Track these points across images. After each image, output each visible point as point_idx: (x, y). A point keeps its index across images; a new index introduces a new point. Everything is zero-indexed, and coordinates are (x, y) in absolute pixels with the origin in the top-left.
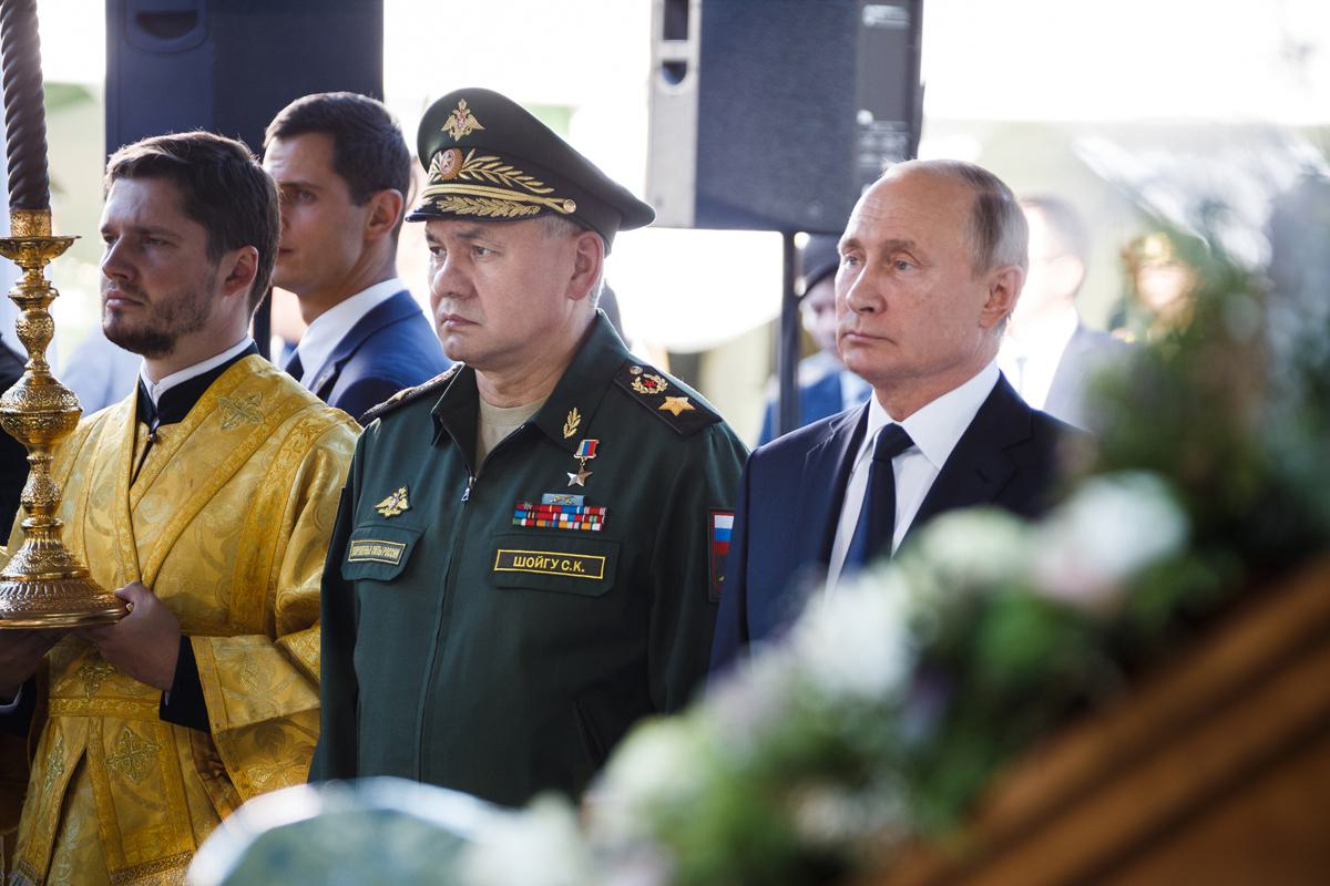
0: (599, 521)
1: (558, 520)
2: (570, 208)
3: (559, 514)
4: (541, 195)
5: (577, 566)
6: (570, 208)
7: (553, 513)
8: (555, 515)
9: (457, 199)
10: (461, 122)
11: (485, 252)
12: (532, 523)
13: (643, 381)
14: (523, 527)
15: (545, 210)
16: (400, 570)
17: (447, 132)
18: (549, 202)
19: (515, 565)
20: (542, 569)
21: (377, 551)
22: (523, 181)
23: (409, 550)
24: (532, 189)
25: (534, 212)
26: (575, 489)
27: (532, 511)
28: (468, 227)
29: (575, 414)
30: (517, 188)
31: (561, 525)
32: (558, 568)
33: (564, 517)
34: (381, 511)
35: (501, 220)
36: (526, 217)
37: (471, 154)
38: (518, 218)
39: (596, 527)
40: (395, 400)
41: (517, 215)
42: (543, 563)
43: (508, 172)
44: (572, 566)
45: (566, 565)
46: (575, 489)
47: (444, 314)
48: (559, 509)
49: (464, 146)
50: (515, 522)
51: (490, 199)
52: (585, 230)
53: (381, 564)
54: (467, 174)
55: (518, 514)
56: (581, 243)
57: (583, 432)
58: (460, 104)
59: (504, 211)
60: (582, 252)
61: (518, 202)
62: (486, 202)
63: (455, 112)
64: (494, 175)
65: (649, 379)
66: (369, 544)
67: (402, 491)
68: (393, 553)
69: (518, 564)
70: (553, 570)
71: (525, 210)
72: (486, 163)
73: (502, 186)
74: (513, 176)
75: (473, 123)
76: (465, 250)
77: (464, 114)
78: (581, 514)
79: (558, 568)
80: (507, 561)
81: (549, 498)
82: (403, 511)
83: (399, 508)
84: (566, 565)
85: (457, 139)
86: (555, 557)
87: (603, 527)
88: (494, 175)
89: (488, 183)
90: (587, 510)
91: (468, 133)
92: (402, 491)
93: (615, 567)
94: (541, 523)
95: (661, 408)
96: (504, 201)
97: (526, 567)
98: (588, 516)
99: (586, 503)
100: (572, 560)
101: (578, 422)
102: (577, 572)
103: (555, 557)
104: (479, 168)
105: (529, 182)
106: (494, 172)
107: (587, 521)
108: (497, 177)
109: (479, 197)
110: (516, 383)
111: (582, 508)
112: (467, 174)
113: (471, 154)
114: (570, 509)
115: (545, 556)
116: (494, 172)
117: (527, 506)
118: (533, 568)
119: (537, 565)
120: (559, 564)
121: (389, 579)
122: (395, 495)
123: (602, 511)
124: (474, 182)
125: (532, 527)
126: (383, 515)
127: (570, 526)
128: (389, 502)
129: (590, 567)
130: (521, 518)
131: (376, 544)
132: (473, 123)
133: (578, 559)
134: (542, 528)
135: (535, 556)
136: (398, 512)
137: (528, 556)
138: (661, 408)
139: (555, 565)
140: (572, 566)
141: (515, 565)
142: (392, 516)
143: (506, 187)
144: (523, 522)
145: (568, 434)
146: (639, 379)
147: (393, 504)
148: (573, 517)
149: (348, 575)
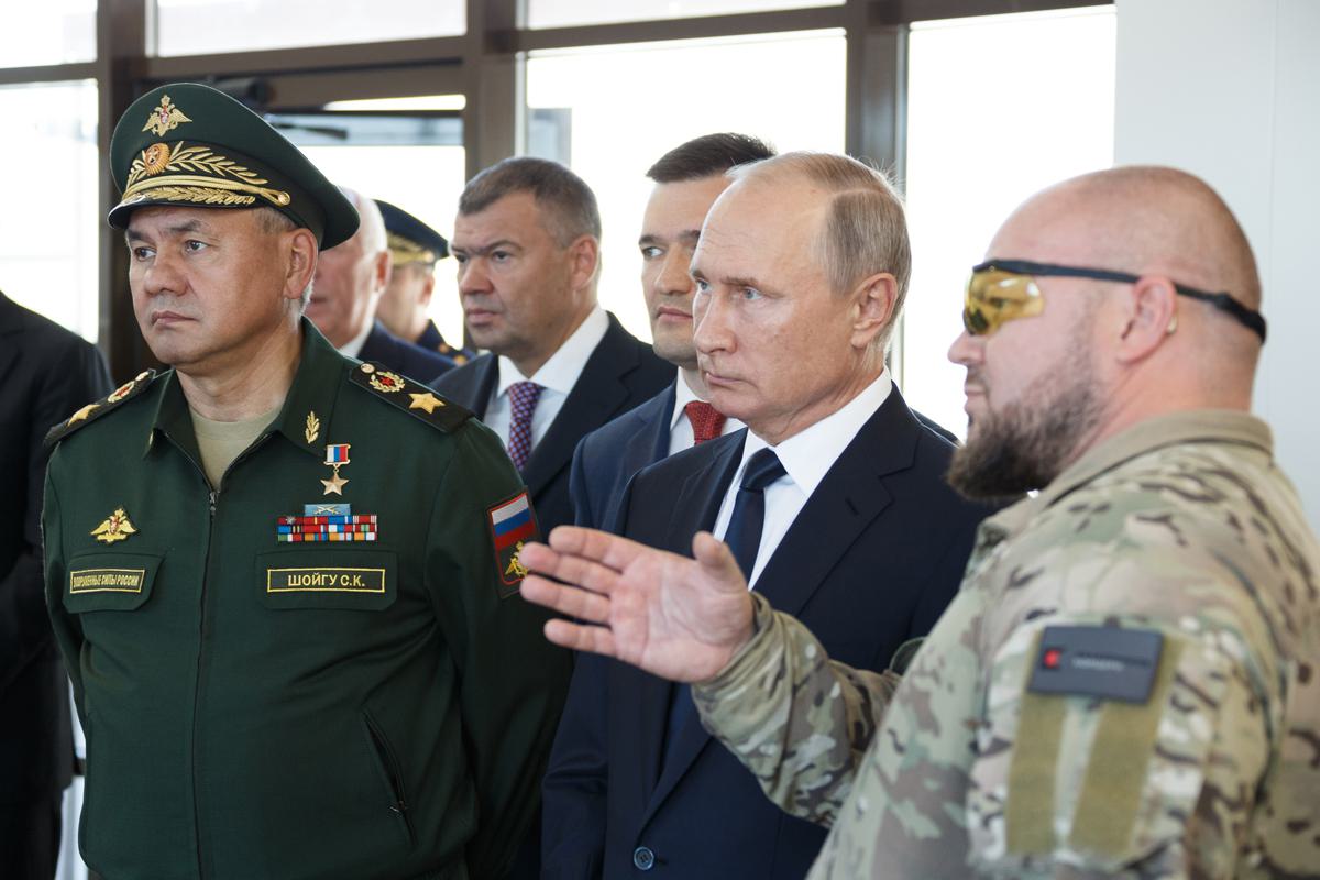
0: (372, 530)
1: (327, 532)
2: (283, 199)
3: (326, 525)
4: (256, 186)
5: (356, 580)
6: (283, 199)
7: (319, 525)
8: (322, 527)
9: (169, 189)
10: (165, 117)
11: (201, 246)
12: (300, 538)
13: (378, 378)
14: (290, 543)
15: (261, 202)
16: (146, 597)
17: (150, 130)
18: (264, 192)
19: (290, 584)
20: (321, 587)
21: (94, 581)
22: (236, 172)
23: (152, 576)
24: (246, 179)
25: (249, 202)
26: (333, 498)
27: (295, 524)
28: (181, 219)
29: (313, 418)
30: (230, 177)
31: (332, 538)
32: (338, 584)
33: (333, 528)
34: (100, 538)
35: (216, 208)
36: (242, 207)
37: (180, 145)
38: (234, 207)
39: (371, 537)
40: (80, 420)
41: (233, 203)
42: (319, 580)
43: (219, 163)
44: (350, 581)
45: (345, 581)
46: (333, 498)
47: (156, 313)
48: (325, 520)
49: (170, 139)
50: (281, 538)
51: (202, 188)
52: (299, 226)
53: (118, 595)
54: (177, 165)
55: (281, 529)
56: (295, 239)
57: (326, 437)
58: (162, 100)
59: (218, 198)
60: (296, 250)
61: (231, 191)
62: (199, 190)
63: (158, 109)
64: (204, 165)
65: (383, 377)
66: (97, 574)
67: (119, 513)
68: (131, 581)
69: (294, 583)
70: (332, 587)
71: (239, 199)
72: (195, 154)
73: (215, 175)
74: (226, 166)
75: (179, 116)
76: (176, 247)
77: (168, 110)
78: (351, 524)
79: (338, 584)
80: (281, 580)
81: (312, 510)
82: (129, 535)
83: (122, 532)
84: (345, 581)
85: (161, 135)
86: (333, 573)
87: (378, 535)
88: (204, 165)
89: (198, 172)
90: (356, 519)
91: (173, 127)
92: (119, 513)
93: (402, 592)
94: (309, 538)
95: (346, 481)
96: (217, 189)
97: (302, 586)
98: (358, 525)
99: (353, 512)
100: (351, 574)
101: (317, 425)
102: (357, 587)
103: (333, 573)
104: (189, 158)
105: (242, 172)
106: (205, 162)
107: (358, 531)
108: (208, 166)
109: (191, 186)
110: (233, 389)
111: (351, 516)
112: (177, 165)
113: (180, 145)
114: (338, 520)
115: (322, 573)
116: (205, 162)
117: (290, 520)
118: (311, 586)
119: (314, 583)
120: (338, 580)
121: (133, 608)
122: (112, 518)
123: (374, 519)
124: (184, 172)
125: (299, 543)
126: (104, 541)
127: (341, 537)
128: (105, 526)
129: (371, 580)
130: (287, 534)
131: (105, 573)
132: (179, 116)
133: (357, 573)
134: (309, 542)
135: (311, 573)
136: (123, 537)
137: (303, 573)
138: (346, 481)
139: (334, 581)
140: (351, 581)
141: (290, 584)
142: (116, 542)
143: (217, 176)
144: (290, 538)
145: (312, 439)
146: (373, 377)
147: (115, 528)
148: (342, 528)
149: (72, 608)
